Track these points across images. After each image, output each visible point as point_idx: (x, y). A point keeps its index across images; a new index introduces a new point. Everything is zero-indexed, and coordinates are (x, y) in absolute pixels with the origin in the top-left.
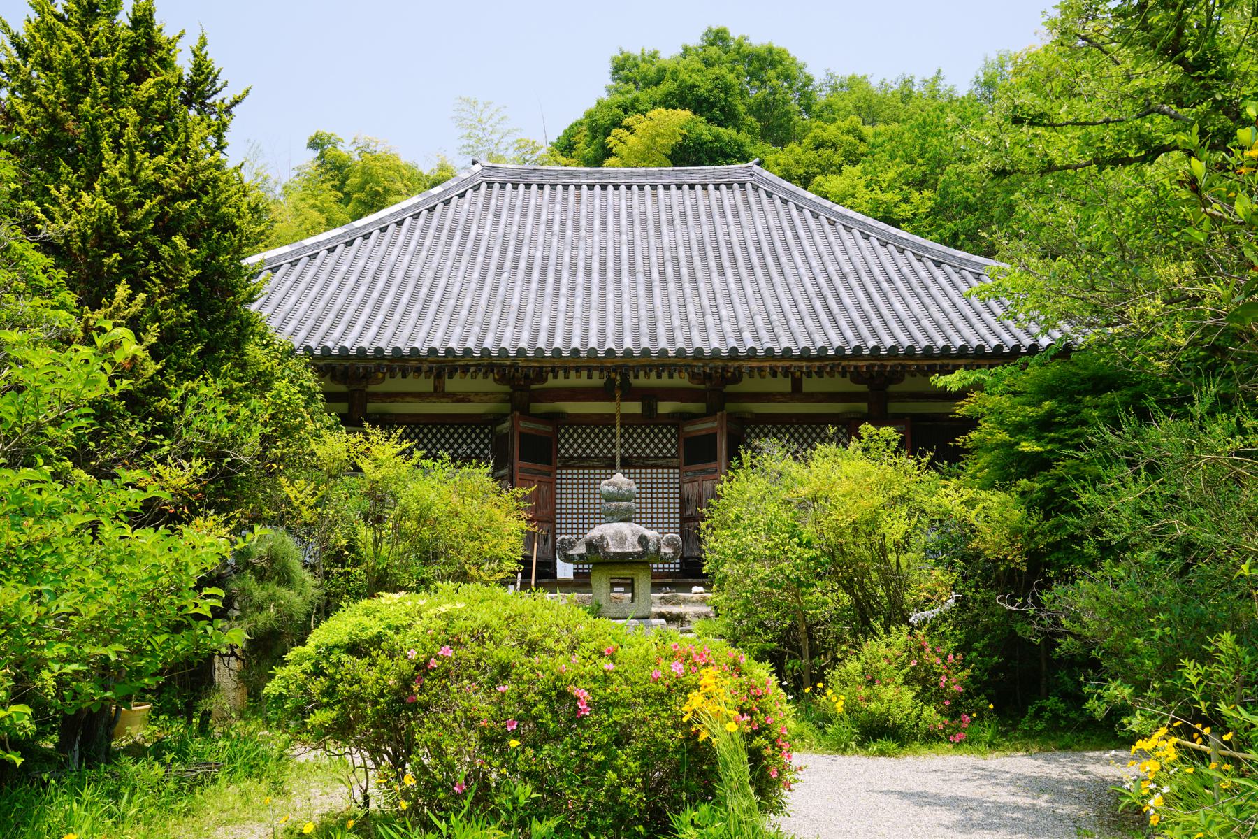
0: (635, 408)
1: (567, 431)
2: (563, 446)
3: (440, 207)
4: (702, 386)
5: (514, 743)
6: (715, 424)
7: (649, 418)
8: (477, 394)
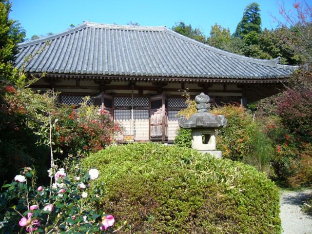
0: (136, 92)
3: (75, 33)
5: (305, 177)
6: (161, 97)
7: (141, 95)
8: (89, 87)
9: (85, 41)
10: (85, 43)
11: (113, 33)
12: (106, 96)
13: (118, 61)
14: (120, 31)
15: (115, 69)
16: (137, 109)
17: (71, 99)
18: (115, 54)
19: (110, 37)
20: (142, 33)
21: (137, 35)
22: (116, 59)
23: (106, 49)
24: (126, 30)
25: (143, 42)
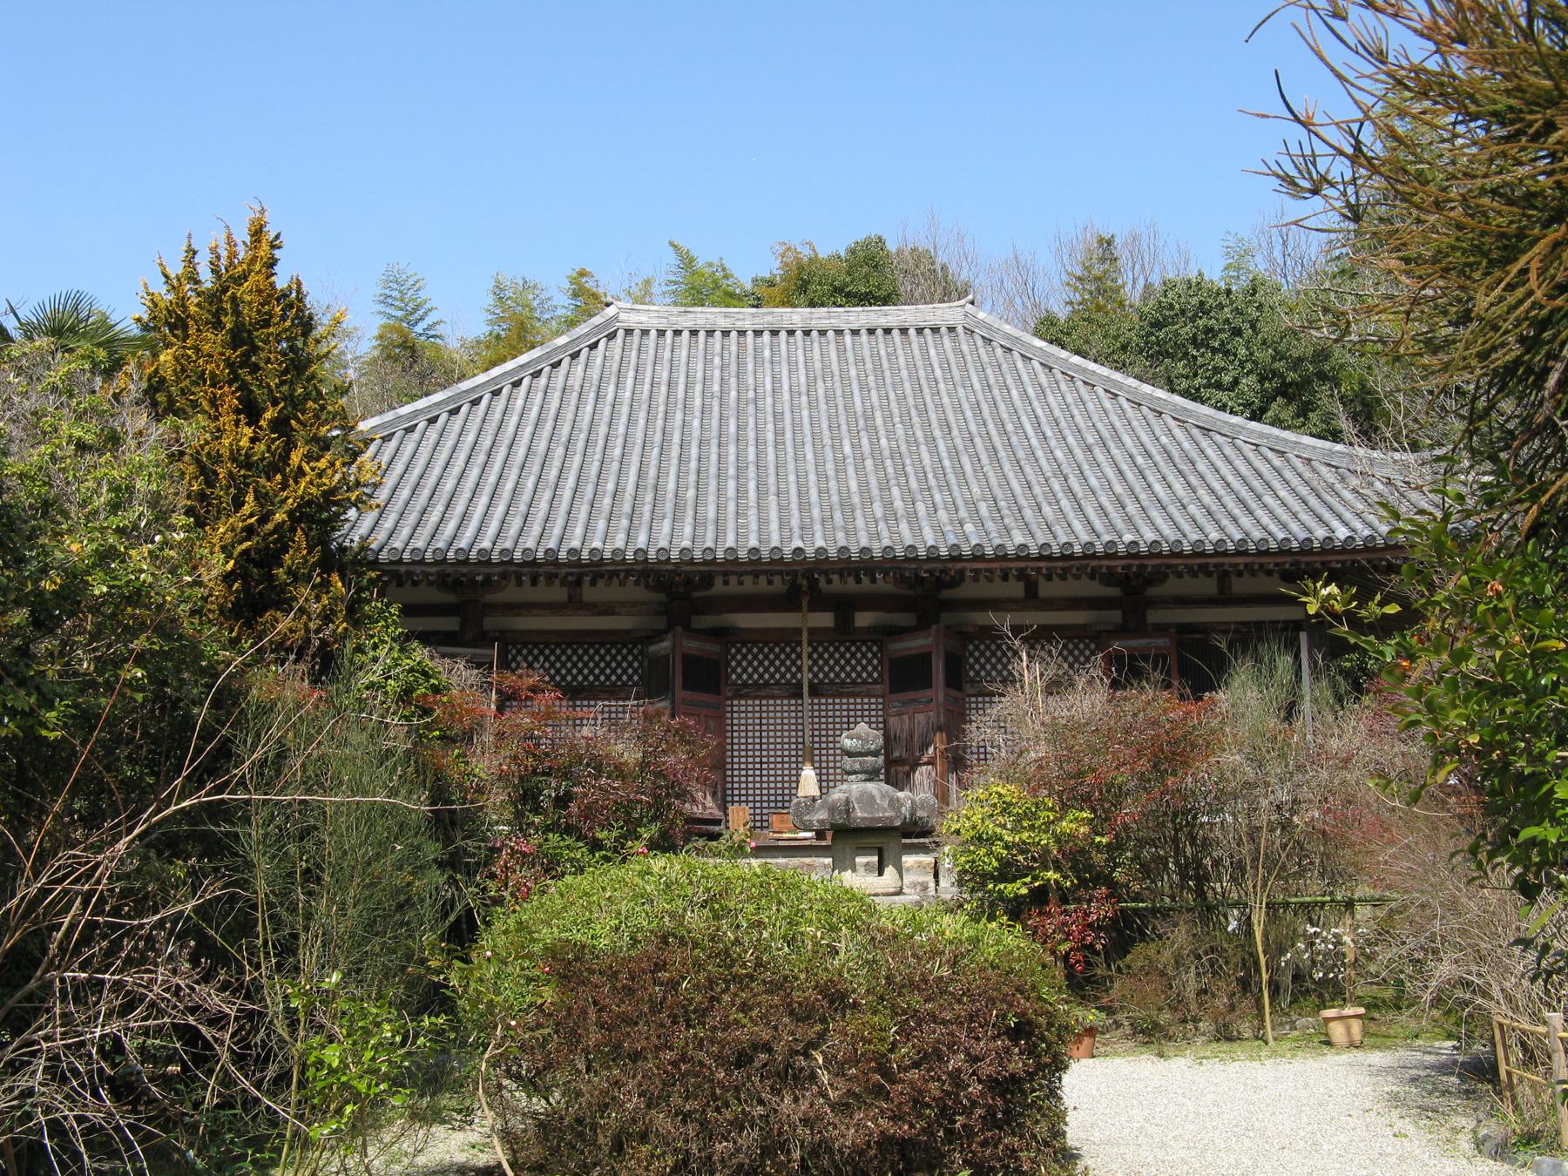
0: (825, 620)
1: (739, 651)
2: (734, 671)
4: (911, 592)
6: (930, 641)
7: (844, 632)
8: (623, 604)
9: (610, 397)
10: (607, 410)
11: (734, 348)
12: (692, 645)
13: (741, 492)
14: (766, 337)
15: (916, 529)
16: (834, 696)
17: (602, 658)
18: (732, 458)
19: (717, 373)
20: (864, 337)
21: (841, 351)
22: (732, 484)
23: (696, 433)
24: (791, 333)
25: (864, 386)
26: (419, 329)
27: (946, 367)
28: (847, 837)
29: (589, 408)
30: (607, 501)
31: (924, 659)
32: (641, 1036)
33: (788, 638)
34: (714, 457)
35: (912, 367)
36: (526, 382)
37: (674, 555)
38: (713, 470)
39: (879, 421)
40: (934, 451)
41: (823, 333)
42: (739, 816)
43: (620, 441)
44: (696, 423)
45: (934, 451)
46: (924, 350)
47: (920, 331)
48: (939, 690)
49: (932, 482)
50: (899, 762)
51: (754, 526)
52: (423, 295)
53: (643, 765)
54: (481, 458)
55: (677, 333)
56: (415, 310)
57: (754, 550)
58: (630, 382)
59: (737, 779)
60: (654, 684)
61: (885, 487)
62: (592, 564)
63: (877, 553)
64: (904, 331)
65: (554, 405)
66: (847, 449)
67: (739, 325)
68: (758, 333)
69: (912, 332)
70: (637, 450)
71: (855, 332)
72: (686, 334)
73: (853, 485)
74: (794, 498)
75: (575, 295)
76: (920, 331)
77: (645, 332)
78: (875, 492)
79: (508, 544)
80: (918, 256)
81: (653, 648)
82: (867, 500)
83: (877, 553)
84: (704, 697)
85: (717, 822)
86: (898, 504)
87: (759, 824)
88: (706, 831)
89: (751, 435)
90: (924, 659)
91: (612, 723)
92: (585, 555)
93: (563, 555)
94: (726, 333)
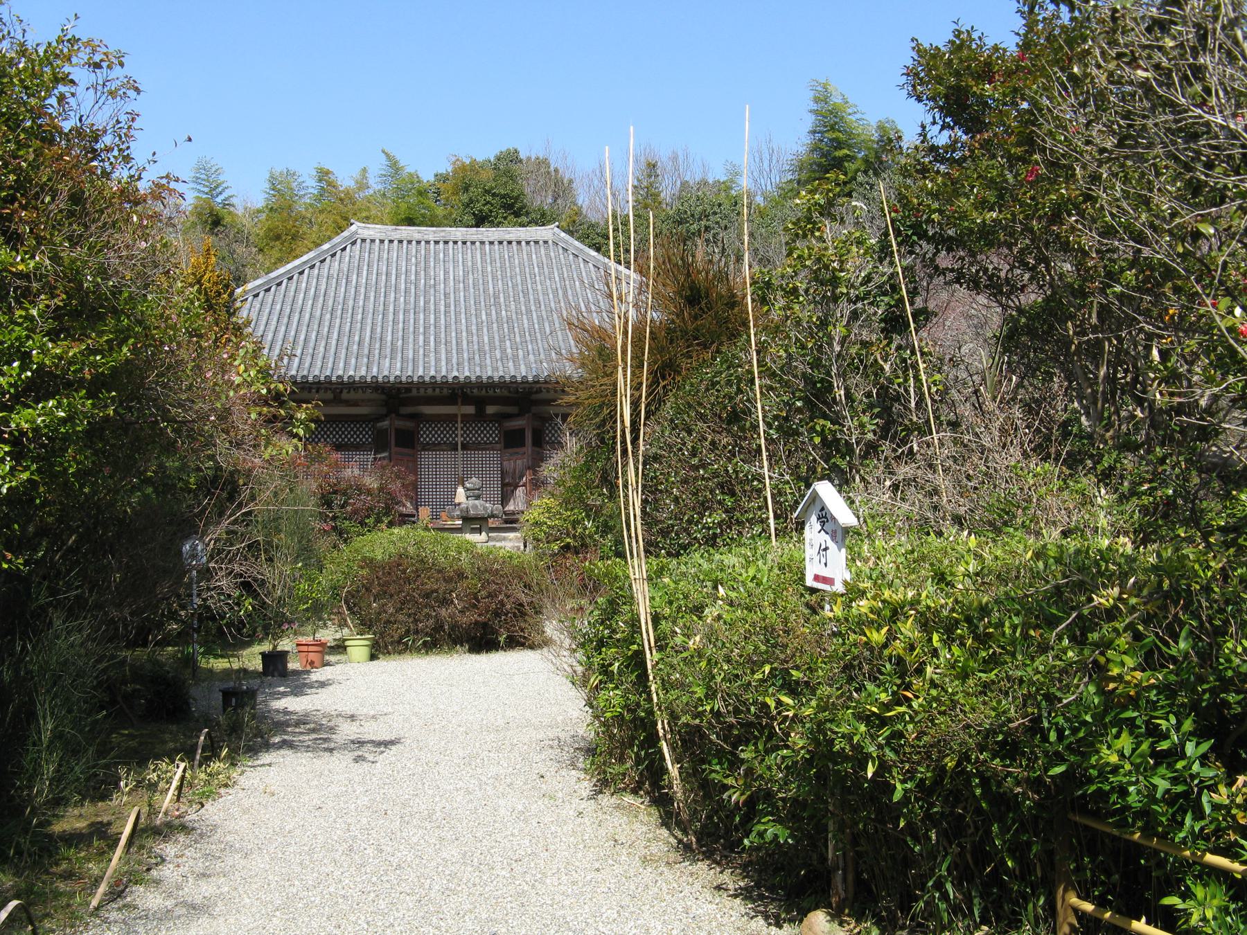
0: (470, 410)
7: (480, 416)
12: (399, 423)
13: (426, 342)
14: (441, 244)
15: (517, 366)
18: (422, 322)
20: (496, 246)
21: (483, 254)
22: (421, 338)
23: (402, 306)
24: (455, 242)
26: (219, 200)
27: (541, 267)
28: (474, 522)
29: (343, 289)
30: (355, 347)
31: (521, 432)
32: (392, 589)
33: (451, 419)
34: (412, 321)
35: (521, 264)
36: (306, 272)
37: (392, 379)
38: (411, 329)
39: (502, 300)
40: (530, 319)
41: (473, 243)
42: (425, 513)
43: (360, 310)
44: (402, 299)
45: (530, 319)
46: (529, 255)
47: (528, 243)
48: (529, 447)
49: (528, 338)
50: (508, 484)
51: (433, 363)
52: (222, 178)
53: (381, 489)
54: (286, 320)
55: (391, 241)
56: (216, 187)
57: (433, 377)
58: (365, 273)
59: (424, 493)
60: (379, 444)
61: (502, 341)
62: (349, 383)
63: (496, 379)
64: (519, 243)
65: (323, 287)
66: (484, 317)
67: (426, 237)
68: (437, 242)
69: (523, 243)
70: (370, 316)
71: (491, 243)
72: (396, 242)
73: (486, 339)
74: (454, 347)
75: (320, 181)
76: (528, 243)
77: (373, 241)
78: (497, 343)
79: (305, 373)
80: (542, 163)
81: (379, 424)
82: (493, 348)
83: (496, 379)
84: (406, 450)
85: (413, 516)
86: (509, 350)
87: (435, 517)
88: (404, 519)
89: (432, 308)
90: (521, 432)
91: (363, 468)
92: (345, 379)
93: (334, 379)
94: (418, 242)
